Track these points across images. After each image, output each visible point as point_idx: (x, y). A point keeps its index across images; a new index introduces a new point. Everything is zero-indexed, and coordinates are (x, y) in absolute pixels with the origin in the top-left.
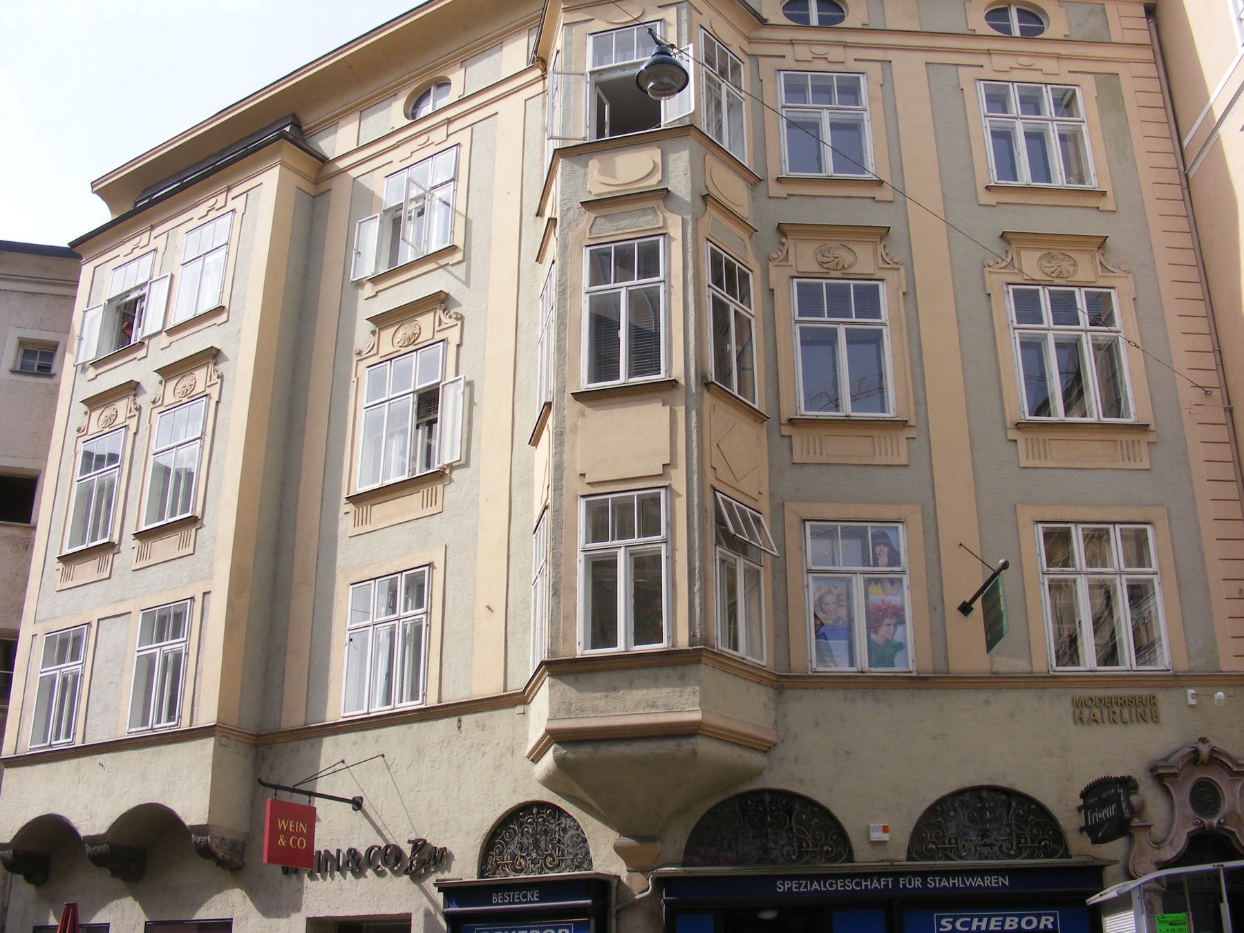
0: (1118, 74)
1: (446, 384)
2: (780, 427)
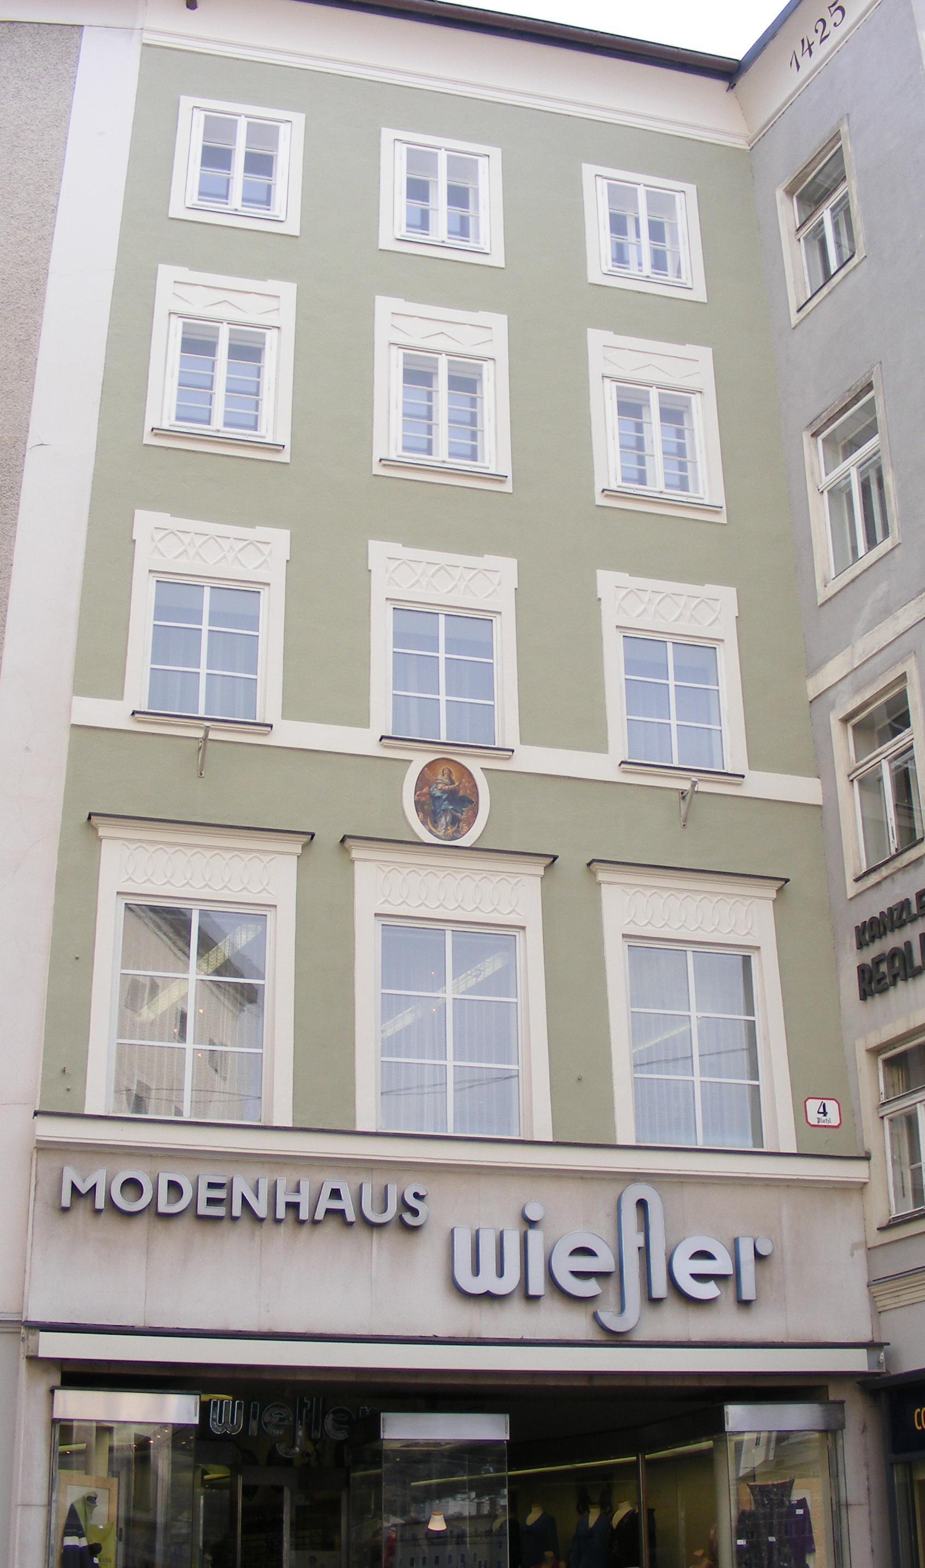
0: (271, 726)
1: (182, 852)
2: (603, 380)
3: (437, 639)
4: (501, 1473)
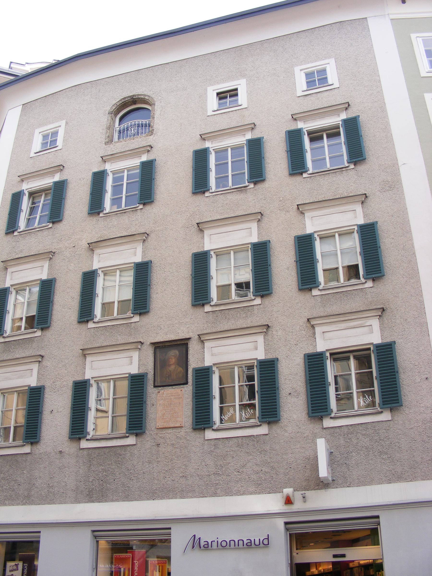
3: (223, 404)
4: (159, 368)
